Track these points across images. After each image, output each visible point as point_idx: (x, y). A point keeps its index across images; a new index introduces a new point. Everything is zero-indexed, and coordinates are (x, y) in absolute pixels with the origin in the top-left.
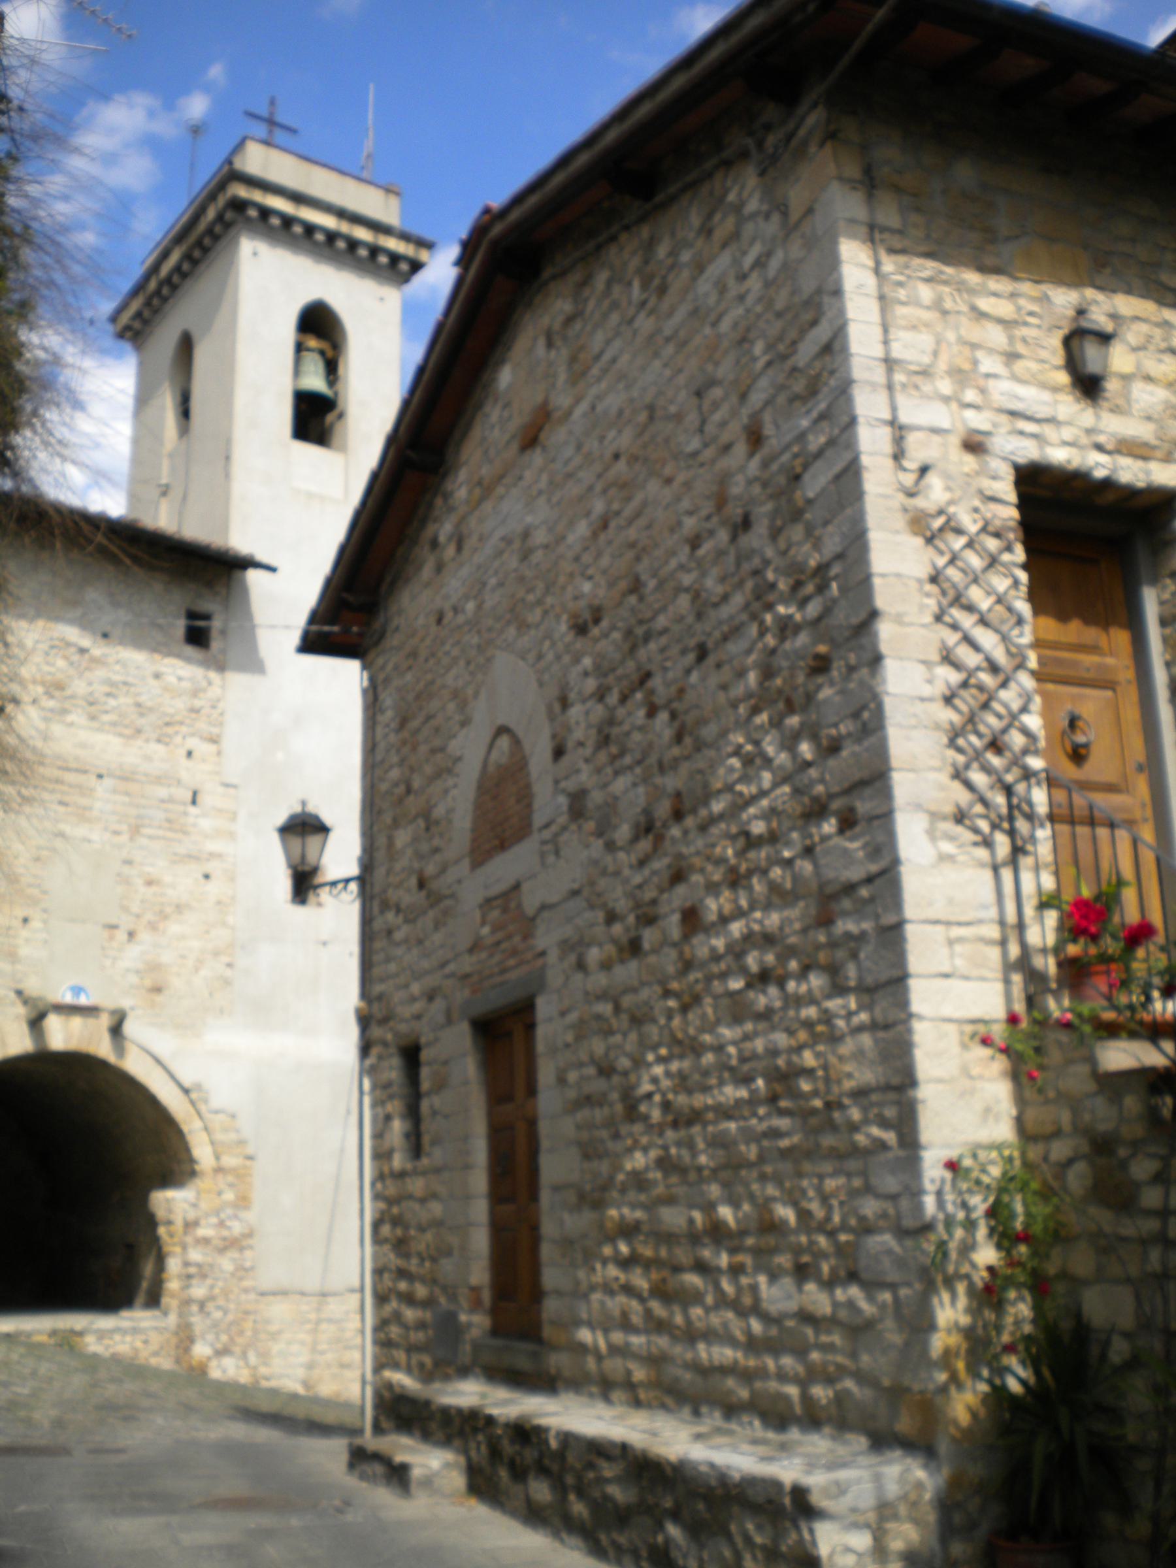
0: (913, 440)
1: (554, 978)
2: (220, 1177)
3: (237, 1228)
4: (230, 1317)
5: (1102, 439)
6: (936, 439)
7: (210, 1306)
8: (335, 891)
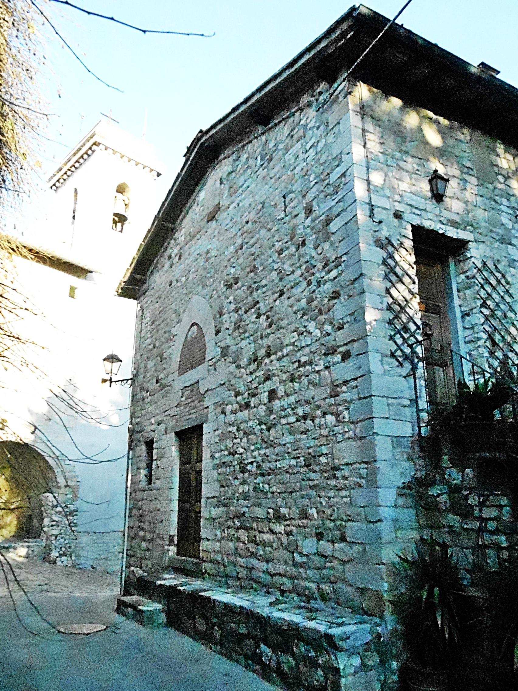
4: (66, 542)
8: (123, 383)
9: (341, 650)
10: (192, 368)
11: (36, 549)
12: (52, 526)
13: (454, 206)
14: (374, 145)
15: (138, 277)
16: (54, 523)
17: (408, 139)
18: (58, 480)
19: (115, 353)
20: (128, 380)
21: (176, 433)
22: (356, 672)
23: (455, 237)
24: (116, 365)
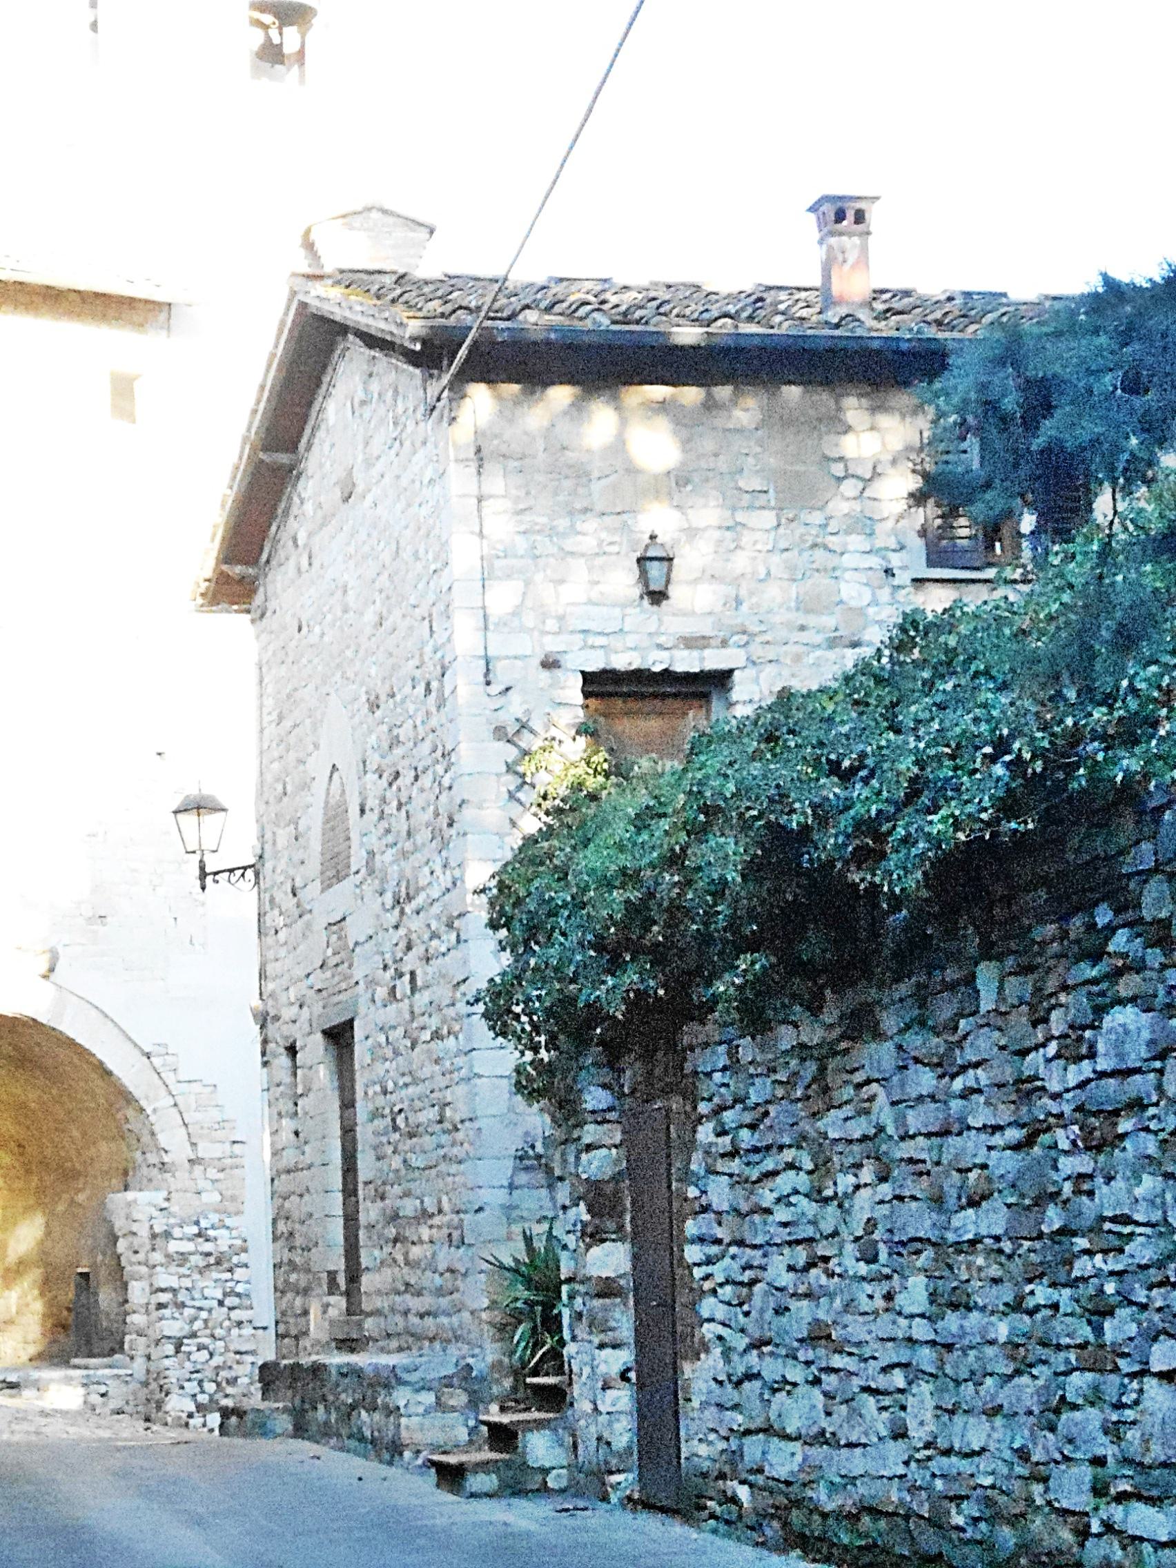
0: (499, 667)
1: (362, 1010)
2: (198, 1169)
3: (224, 1241)
4: (217, 1360)
5: (662, 640)
6: (519, 663)
7: (190, 1346)
8: (233, 879)
9: (406, 1383)
10: (339, 881)
11: (114, 1388)
12: (161, 1306)
13: (693, 599)
14: (501, 525)
15: (238, 569)
16: (164, 1297)
17: (596, 474)
18: (163, 1140)
19: (206, 791)
20: (245, 868)
21: (324, 1032)
22: (427, 1412)
23: (697, 670)
24: (210, 819)
